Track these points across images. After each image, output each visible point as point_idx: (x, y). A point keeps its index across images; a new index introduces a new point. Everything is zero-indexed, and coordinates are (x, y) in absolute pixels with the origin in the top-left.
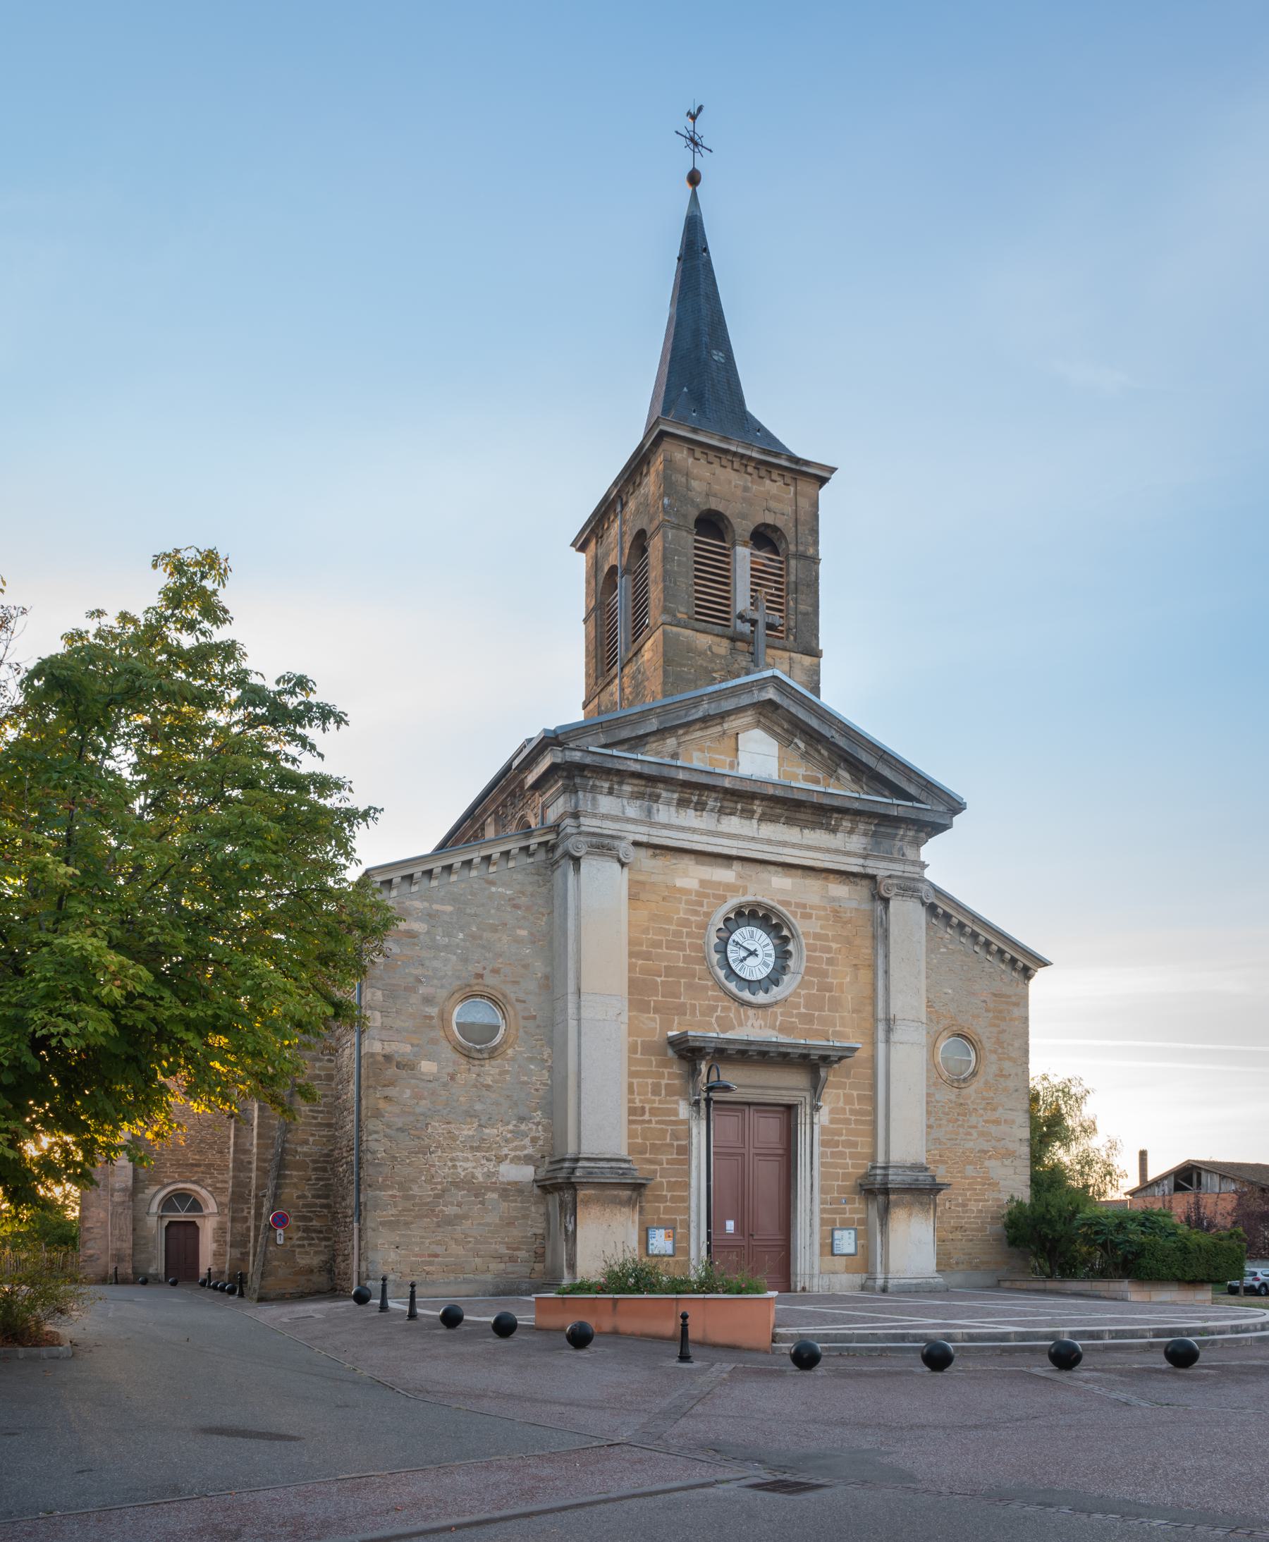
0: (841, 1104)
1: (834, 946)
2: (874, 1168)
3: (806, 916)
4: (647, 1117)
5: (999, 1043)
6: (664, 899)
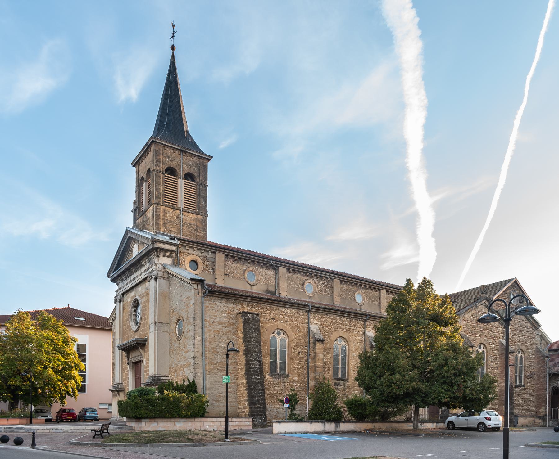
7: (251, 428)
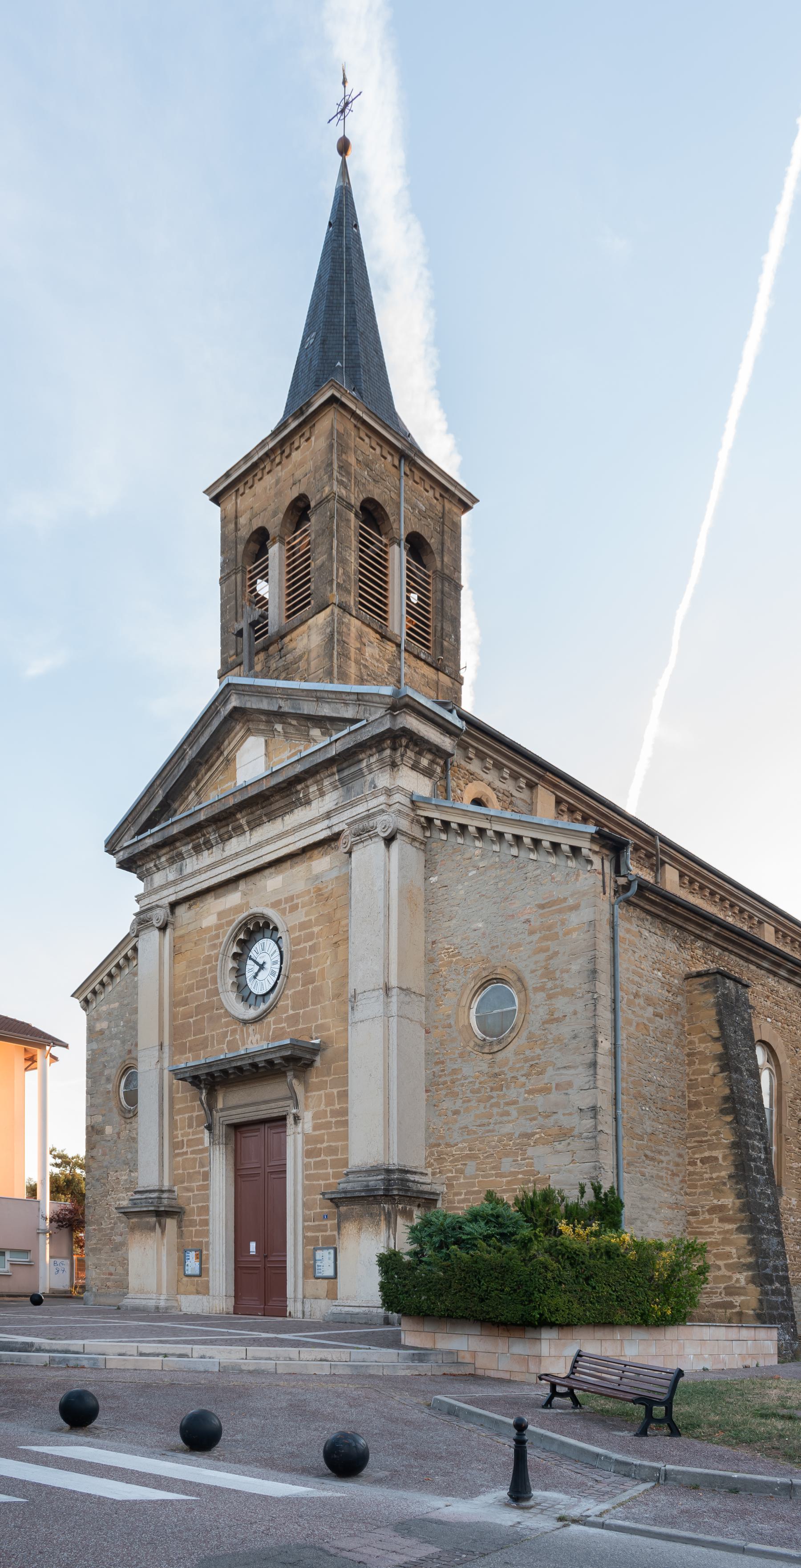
0: (323, 1107)
1: (316, 929)
5: (549, 974)
7: (774, 1361)
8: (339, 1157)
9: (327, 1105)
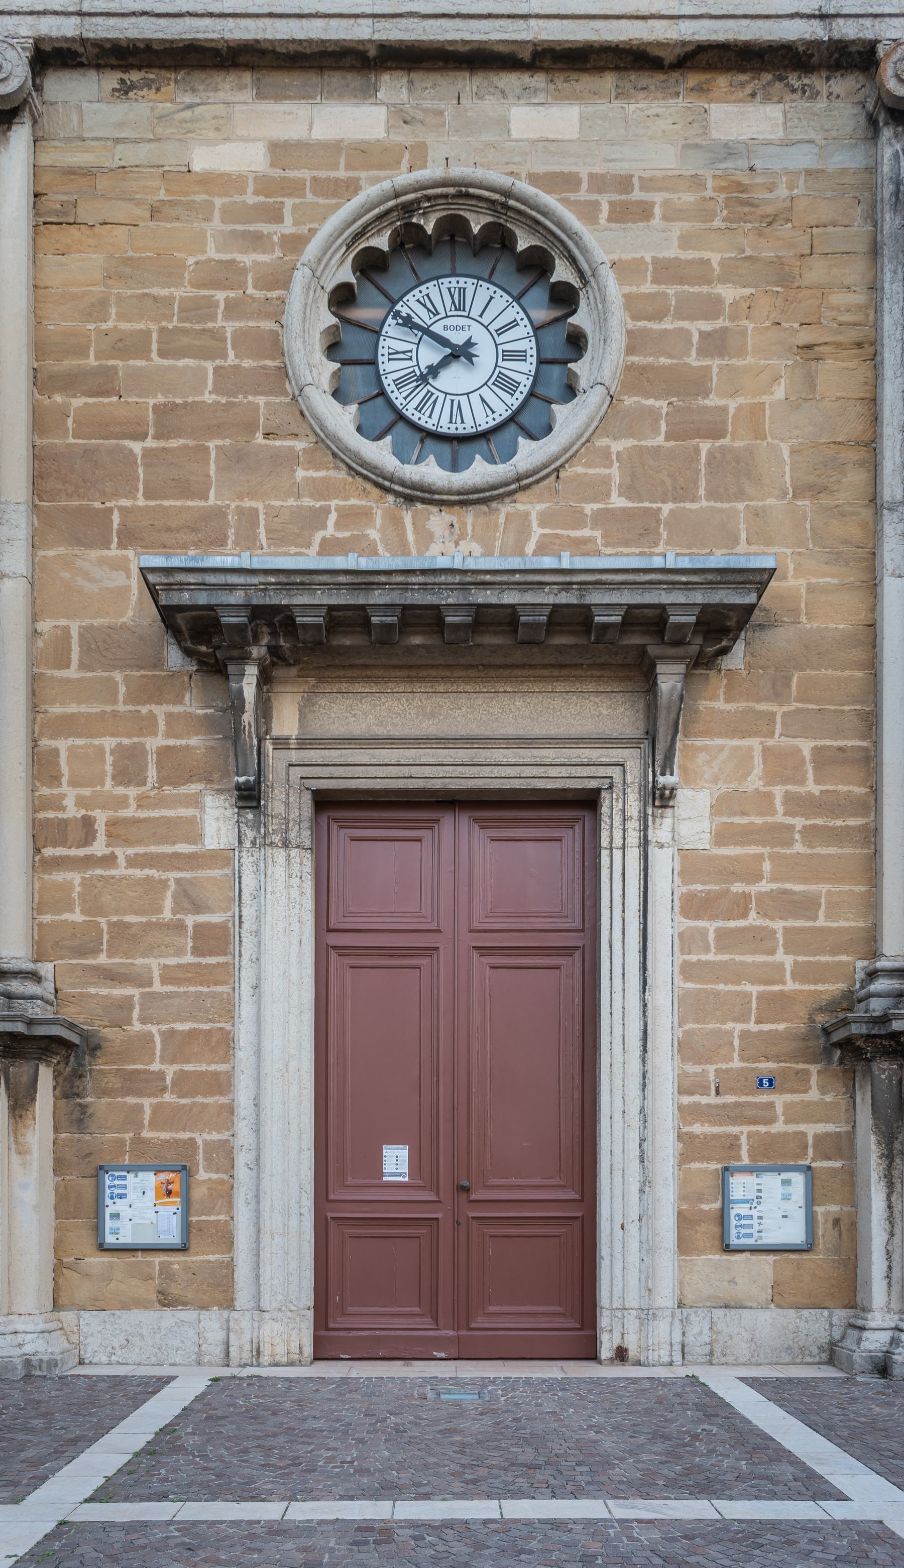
0: (755, 781)
2: (872, 975)
3: (631, 213)
4: (99, 848)
6: (155, 212)
8: (821, 922)
9: (771, 778)
